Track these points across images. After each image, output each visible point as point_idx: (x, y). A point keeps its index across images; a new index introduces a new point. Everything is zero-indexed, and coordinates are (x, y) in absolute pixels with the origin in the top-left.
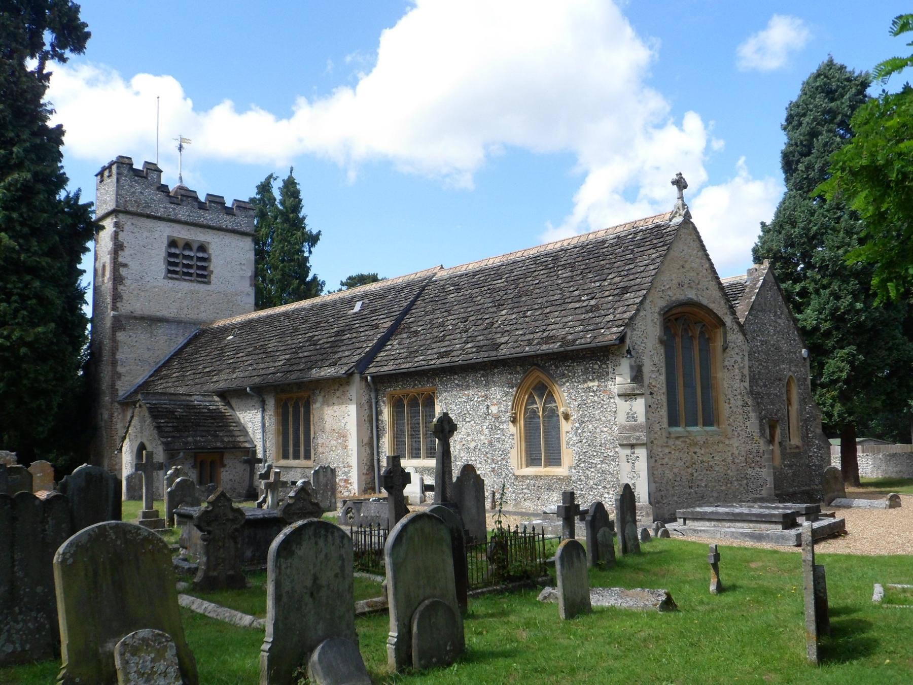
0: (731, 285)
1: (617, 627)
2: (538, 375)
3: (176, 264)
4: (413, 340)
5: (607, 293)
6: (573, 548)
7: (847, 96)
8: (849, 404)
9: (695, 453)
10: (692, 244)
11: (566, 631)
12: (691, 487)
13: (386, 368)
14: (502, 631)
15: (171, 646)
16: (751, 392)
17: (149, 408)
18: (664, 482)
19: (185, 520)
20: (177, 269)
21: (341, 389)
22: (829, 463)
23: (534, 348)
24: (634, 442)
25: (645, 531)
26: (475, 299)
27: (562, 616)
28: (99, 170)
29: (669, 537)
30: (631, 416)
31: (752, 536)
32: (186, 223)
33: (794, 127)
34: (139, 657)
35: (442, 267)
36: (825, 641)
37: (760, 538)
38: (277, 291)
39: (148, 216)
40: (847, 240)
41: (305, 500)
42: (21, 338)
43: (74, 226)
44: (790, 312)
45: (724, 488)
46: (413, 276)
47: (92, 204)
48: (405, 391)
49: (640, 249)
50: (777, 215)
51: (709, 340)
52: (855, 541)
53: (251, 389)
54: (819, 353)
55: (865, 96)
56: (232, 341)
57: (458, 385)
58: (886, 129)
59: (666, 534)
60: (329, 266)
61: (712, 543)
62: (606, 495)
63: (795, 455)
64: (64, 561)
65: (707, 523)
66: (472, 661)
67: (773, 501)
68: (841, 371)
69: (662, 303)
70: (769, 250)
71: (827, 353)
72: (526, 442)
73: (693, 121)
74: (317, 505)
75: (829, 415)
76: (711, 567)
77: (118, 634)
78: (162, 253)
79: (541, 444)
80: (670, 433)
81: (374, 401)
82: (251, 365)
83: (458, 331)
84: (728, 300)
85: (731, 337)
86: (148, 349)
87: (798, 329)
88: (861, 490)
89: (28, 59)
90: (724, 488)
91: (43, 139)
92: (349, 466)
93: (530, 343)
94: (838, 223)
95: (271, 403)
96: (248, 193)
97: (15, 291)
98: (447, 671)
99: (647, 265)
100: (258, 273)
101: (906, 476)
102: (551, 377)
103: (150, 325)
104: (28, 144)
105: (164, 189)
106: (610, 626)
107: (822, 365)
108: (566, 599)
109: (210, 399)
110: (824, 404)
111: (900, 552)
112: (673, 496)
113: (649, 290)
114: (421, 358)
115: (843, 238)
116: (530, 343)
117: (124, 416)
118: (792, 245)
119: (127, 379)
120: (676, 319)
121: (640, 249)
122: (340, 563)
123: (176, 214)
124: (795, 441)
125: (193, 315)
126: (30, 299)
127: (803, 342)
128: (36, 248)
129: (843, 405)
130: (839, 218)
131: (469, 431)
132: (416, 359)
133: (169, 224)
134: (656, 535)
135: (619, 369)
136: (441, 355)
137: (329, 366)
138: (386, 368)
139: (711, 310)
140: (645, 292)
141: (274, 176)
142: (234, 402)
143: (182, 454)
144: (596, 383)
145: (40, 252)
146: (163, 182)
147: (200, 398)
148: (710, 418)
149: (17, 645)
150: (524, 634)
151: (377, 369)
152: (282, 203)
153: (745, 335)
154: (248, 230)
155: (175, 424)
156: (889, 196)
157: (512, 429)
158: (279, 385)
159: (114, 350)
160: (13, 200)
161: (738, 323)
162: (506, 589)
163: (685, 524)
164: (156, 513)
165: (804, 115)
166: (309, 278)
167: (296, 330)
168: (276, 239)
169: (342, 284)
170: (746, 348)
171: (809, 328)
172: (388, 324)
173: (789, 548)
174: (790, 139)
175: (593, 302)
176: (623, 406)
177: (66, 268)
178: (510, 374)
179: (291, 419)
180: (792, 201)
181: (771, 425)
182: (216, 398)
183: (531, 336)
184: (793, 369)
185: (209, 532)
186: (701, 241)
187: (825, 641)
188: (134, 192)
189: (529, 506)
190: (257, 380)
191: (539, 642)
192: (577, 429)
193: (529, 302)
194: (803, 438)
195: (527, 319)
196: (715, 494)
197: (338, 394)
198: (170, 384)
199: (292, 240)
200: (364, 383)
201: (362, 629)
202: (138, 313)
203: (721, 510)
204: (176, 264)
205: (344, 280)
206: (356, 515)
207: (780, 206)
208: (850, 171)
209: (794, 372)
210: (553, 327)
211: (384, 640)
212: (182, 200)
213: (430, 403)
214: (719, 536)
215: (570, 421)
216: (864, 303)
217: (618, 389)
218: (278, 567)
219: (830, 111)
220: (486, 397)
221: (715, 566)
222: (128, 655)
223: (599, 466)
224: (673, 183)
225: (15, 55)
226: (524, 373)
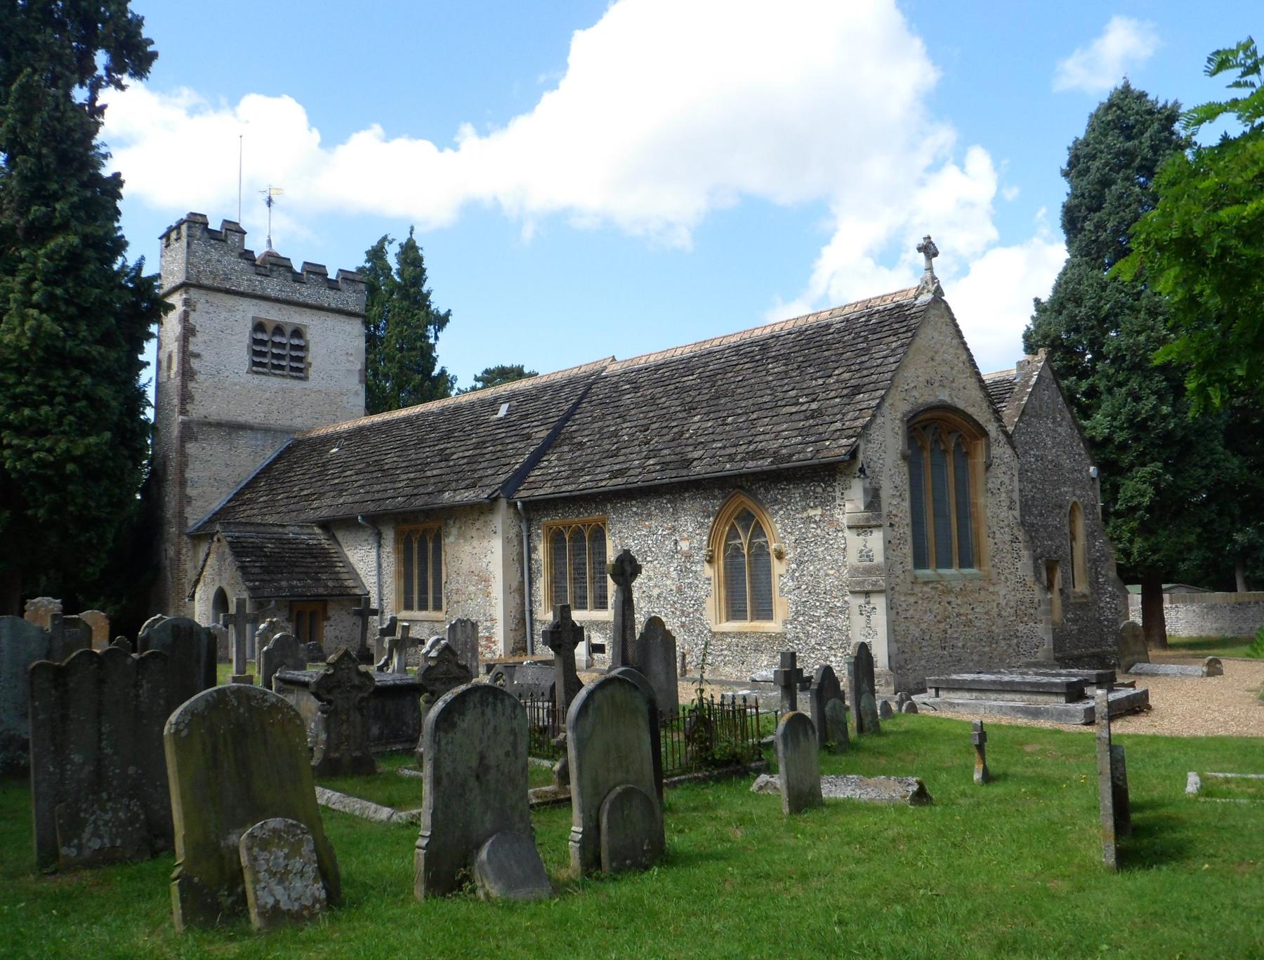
1: (858, 824)
3: (263, 354)
4: (577, 454)
5: (833, 394)
6: (798, 722)
7: (1147, 134)
8: (1153, 539)
9: (949, 603)
10: (944, 328)
11: (791, 829)
13: (541, 492)
14: (709, 829)
16: (1023, 523)
17: (230, 543)
18: (909, 640)
19: (289, 687)
20: (265, 361)
21: (482, 519)
22: (1127, 616)
23: (737, 466)
24: (870, 588)
25: (885, 704)
27: (786, 810)
28: (164, 230)
29: (916, 712)
30: (866, 555)
32: (277, 300)
33: (1079, 172)
34: (270, 852)
35: (614, 359)
36: (1126, 842)
37: (1036, 713)
38: (392, 389)
40: (1151, 322)
42: (68, 450)
43: (136, 305)
44: (1073, 417)
45: (987, 649)
47: (158, 276)
49: (876, 336)
50: (1057, 289)
52: (1162, 718)
54: (1111, 471)
55: (1172, 133)
56: (337, 455)
57: (636, 513)
58: (1202, 191)
59: (913, 708)
60: (460, 356)
61: (977, 721)
62: (832, 658)
63: (1082, 606)
64: (178, 731)
65: (967, 695)
66: (676, 865)
67: (1052, 667)
68: (1142, 496)
69: (904, 407)
70: (1045, 337)
73: (979, 159)
74: (465, 667)
75: (1127, 553)
76: (974, 750)
77: (242, 825)
78: (246, 340)
79: (747, 590)
80: (916, 578)
81: (525, 534)
83: (636, 442)
84: (992, 403)
85: (996, 451)
86: (227, 465)
87: (1084, 440)
88: (1169, 653)
89: (77, 86)
90: (987, 649)
91: (95, 192)
92: (492, 620)
93: (731, 458)
94: (1138, 300)
95: (389, 536)
96: (356, 260)
97: (60, 390)
98: (645, 876)
100: (370, 364)
101: (1229, 635)
102: (760, 503)
103: (230, 434)
104: (76, 199)
105: (247, 255)
106: (848, 823)
107: (1116, 488)
108: (790, 788)
110: (1119, 539)
111: (1222, 733)
112: (920, 659)
116: (731, 458)
117: (196, 554)
118: (1077, 330)
119: (199, 503)
121: (876, 336)
122: (512, 738)
124: (1081, 587)
125: (284, 421)
126: (78, 400)
127: (1092, 457)
129: (1146, 539)
131: (651, 573)
133: (255, 301)
134: (900, 710)
136: (615, 475)
137: (466, 488)
138: (541, 492)
141: (390, 238)
142: (339, 536)
144: (819, 511)
145: (90, 339)
146: (246, 247)
147: (297, 529)
149: (106, 840)
150: (739, 833)
151: (529, 493)
152: (400, 273)
153: (1014, 448)
154: (357, 309)
156: (1204, 275)
157: (708, 571)
158: (400, 513)
159: (183, 465)
160: (57, 272)
161: (1005, 433)
163: (937, 695)
164: (250, 679)
165: (1093, 158)
166: (436, 372)
167: (421, 441)
168: (392, 321)
169: (477, 379)
170: (1015, 464)
171: (1099, 439)
172: (544, 434)
173: (1074, 726)
174: (1074, 188)
175: (814, 406)
176: (854, 541)
177: (124, 360)
179: (415, 557)
180: (1076, 271)
181: (1049, 566)
182: (317, 530)
183: (733, 450)
184: (1078, 492)
185: (330, 702)
186: (956, 326)
187: (1126, 842)
188: (209, 260)
189: (730, 672)
191: (759, 842)
192: (794, 571)
194: (1091, 585)
195: (727, 428)
196: (976, 657)
197: (478, 525)
199: (414, 322)
200: (512, 510)
201: (539, 822)
202: (214, 418)
204: (263, 354)
205: (479, 375)
206: (508, 682)
207: (1060, 278)
208: (1156, 244)
209: (1079, 497)
210: (762, 437)
211: (564, 838)
213: (599, 536)
214: (982, 711)
215: (784, 562)
216: (1173, 406)
217: (849, 519)
218: (436, 742)
219: (1125, 153)
220: (674, 529)
222: (256, 850)
224: (920, 249)
225: (60, 83)
226: (724, 498)
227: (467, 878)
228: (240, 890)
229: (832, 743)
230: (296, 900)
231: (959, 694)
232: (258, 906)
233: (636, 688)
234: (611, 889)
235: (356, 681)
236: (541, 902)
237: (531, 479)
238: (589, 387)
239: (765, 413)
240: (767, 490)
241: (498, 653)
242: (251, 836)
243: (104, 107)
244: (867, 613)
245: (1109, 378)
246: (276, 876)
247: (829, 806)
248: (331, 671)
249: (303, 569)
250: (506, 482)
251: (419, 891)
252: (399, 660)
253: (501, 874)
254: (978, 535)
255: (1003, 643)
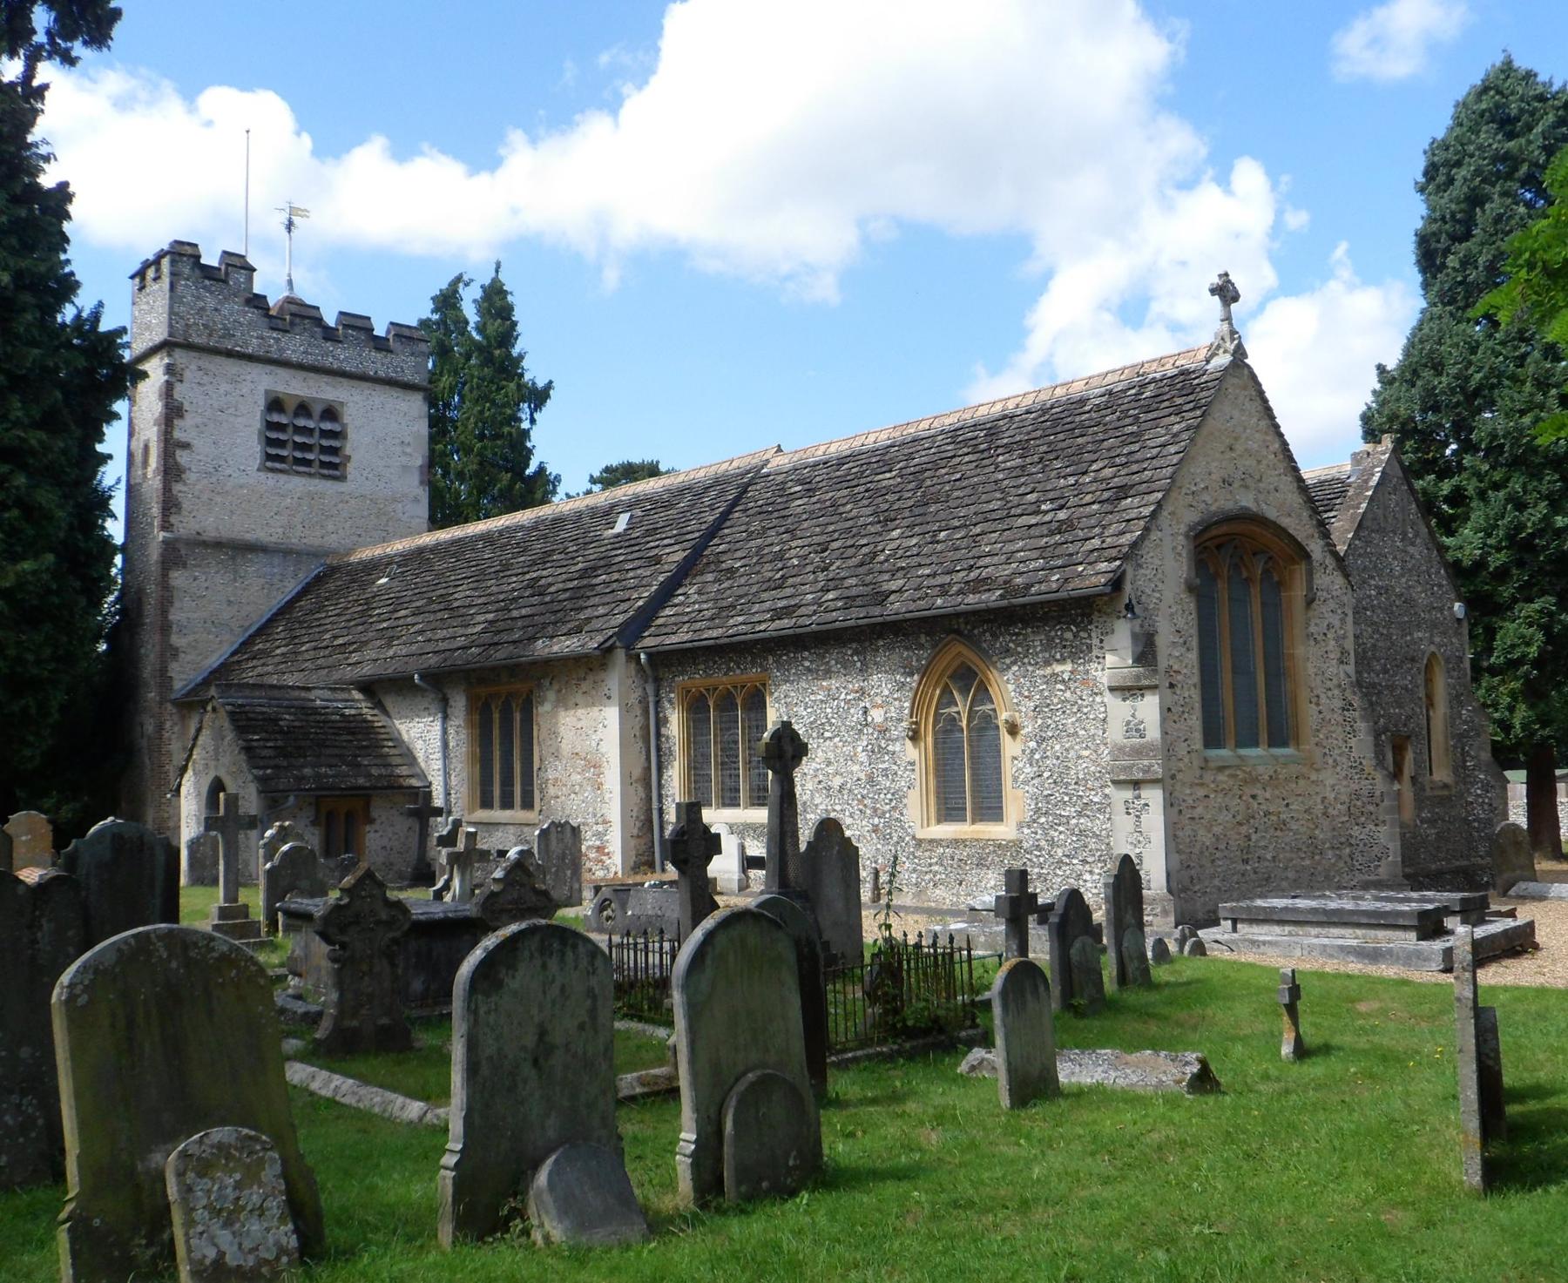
0: (1322, 483)
1: (1108, 1123)
2: (959, 651)
5: (1088, 498)
6: (1024, 976)
7: (1539, 129)
8: (1542, 705)
9: (1254, 797)
10: (1248, 405)
11: (1012, 1131)
12: (1246, 861)
13: (674, 639)
14: (892, 1130)
15: (272, 1160)
16: (1359, 684)
17: (231, 714)
18: (1196, 851)
20: (284, 453)
21: (591, 677)
22: (1505, 815)
23: (952, 601)
24: (1140, 776)
26: (842, 509)
27: (1005, 1102)
28: (136, 266)
29: (1204, 954)
30: (1134, 729)
31: (1361, 953)
32: (300, 367)
33: (1438, 187)
34: (213, 1179)
35: (779, 450)
36: (1496, 1149)
37: (1375, 956)
38: (470, 494)
39: (230, 354)
40: (1539, 398)
41: (522, 885)
43: (91, 371)
44: (1431, 533)
46: (725, 466)
48: (710, 681)
49: (1150, 416)
50: (1408, 352)
51: (1280, 586)
53: (422, 677)
54: (1485, 611)
56: (387, 589)
57: (809, 670)
59: (1199, 949)
60: (569, 448)
62: (1087, 876)
63: (1443, 801)
65: (1277, 929)
66: (837, 1188)
68: (1528, 644)
69: (1192, 517)
70: (1393, 418)
71: (1502, 609)
72: (937, 776)
73: (1249, 176)
74: (545, 894)
75: (1505, 726)
77: (172, 1137)
78: (256, 423)
79: (965, 782)
80: (1206, 760)
81: (651, 699)
82: (421, 632)
83: (810, 568)
84: (1315, 512)
85: (1321, 580)
86: (230, 603)
87: (1447, 565)
90: (1308, 862)
91: (31, 210)
92: (605, 822)
93: (944, 590)
94: (1522, 366)
95: (459, 703)
96: (416, 310)
98: (789, 1205)
99: (1163, 446)
100: (435, 459)
103: (233, 558)
105: (258, 302)
106: (1095, 1122)
107: (1491, 633)
108: (1011, 1070)
109: (345, 696)
110: (1495, 705)
112: (1213, 877)
113: (1167, 491)
114: (740, 619)
115: (1531, 395)
116: (944, 590)
117: (185, 728)
118: (1436, 408)
119: (189, 658)
120: (1218, 547)
121: (1150, 416)
122: (589, 1002)
123: (281, 350)
124: (1442, 775)
125: (313, 539)
128: (19, 414)
129: (1531, 707)
130: (1524, 356)
131: (831, 755)
132: (731, 622)
133: (269, 368)
135: (1110, 641)
136: (778, 614)
139: (1284, 530)
140: (1160, 495)
141: (465, 278)
142: (389, 702)
143: (292, 799)
144: (1068, 667)
145: (26, 421)
146: (257, 289)
147: (327, 694)
148: (1282, 732)
150: (934, 1136)
151: (658, 640)
152: (480, 329)
153: (1347, 576)
154: (417, 380)
155: (280, 743)
157: (911, 752)
158: (474, 670)
159: (166, 603)
161: (1335, 554)
162: (900, 1053)
163: (1235, 930)
164: (244, 911)
165: (1458, 164)
166: (530, 471)
167: (506, 567)
169: (593, 481)
170: (1349, 599)
171: (1467, 563)
173: (1429, 975)
174: (1432, 209)
175: (1062, 515)
176: (1119, 709)
177: (75, 450)
178: (907, 649)
179: (496, 732)
181: (1395, 745)
182: (357, 695)
183: (947, 579)
184: (1437, 639)
185: (343, 946)
186: (1265, 401)
188: (203, 309)
189: (942, 896)
190: (433, 660)
192: (1033, 752)
193: (942, 515)
194: (1455, 770)
195: (939, 547)
196: (1291, 874)
197: (585, 686)
198: (270, 668)
199: (499, 398)
200: (633, 665)
201: (630, 1126)
202: (211, 534)
203: (1302, 903)
205: (596, 474)
206: (619, 913)
207: (1413, 335)
209: (1439, 646)
210: (987, 560)
211: (671, 1147)
212: (292, 324)
213: (757, 703)
215: (1019, 738)
217: (1110, 678)
218: (472, 1010)
219: (1506, 157)
220: (862, 692)
221: (1292, 1009)
222: (191, 1176)
223: (1074, 821)
224: (1213, 291)
227: (520, 1213)
228: (166, 1236)
229: (1079, 1001)
230: (251, 1251)
231: (1265, 928)
232: (191, 1261)
233: (780, 927)
234: (735, 1226)
235: (384, 916)
236: (628, 1247)
237: (660, 621)
238: (744, 490)
239: (993, 526)
240: (995, 636)
241: (613, 870)
242: (184, 1155)
243: (45, 87)
244: (1136, 812)
245: (1480, 476)
246: (219, 1212)
247: (1067, 1096)
248: (346, 901)
249: (336, 751)
250: (624, 626)
251: (446, 1232)
252: (462, 881)
253: (567, 1206)
254: (1295, 699)
255: (1330, 854)
